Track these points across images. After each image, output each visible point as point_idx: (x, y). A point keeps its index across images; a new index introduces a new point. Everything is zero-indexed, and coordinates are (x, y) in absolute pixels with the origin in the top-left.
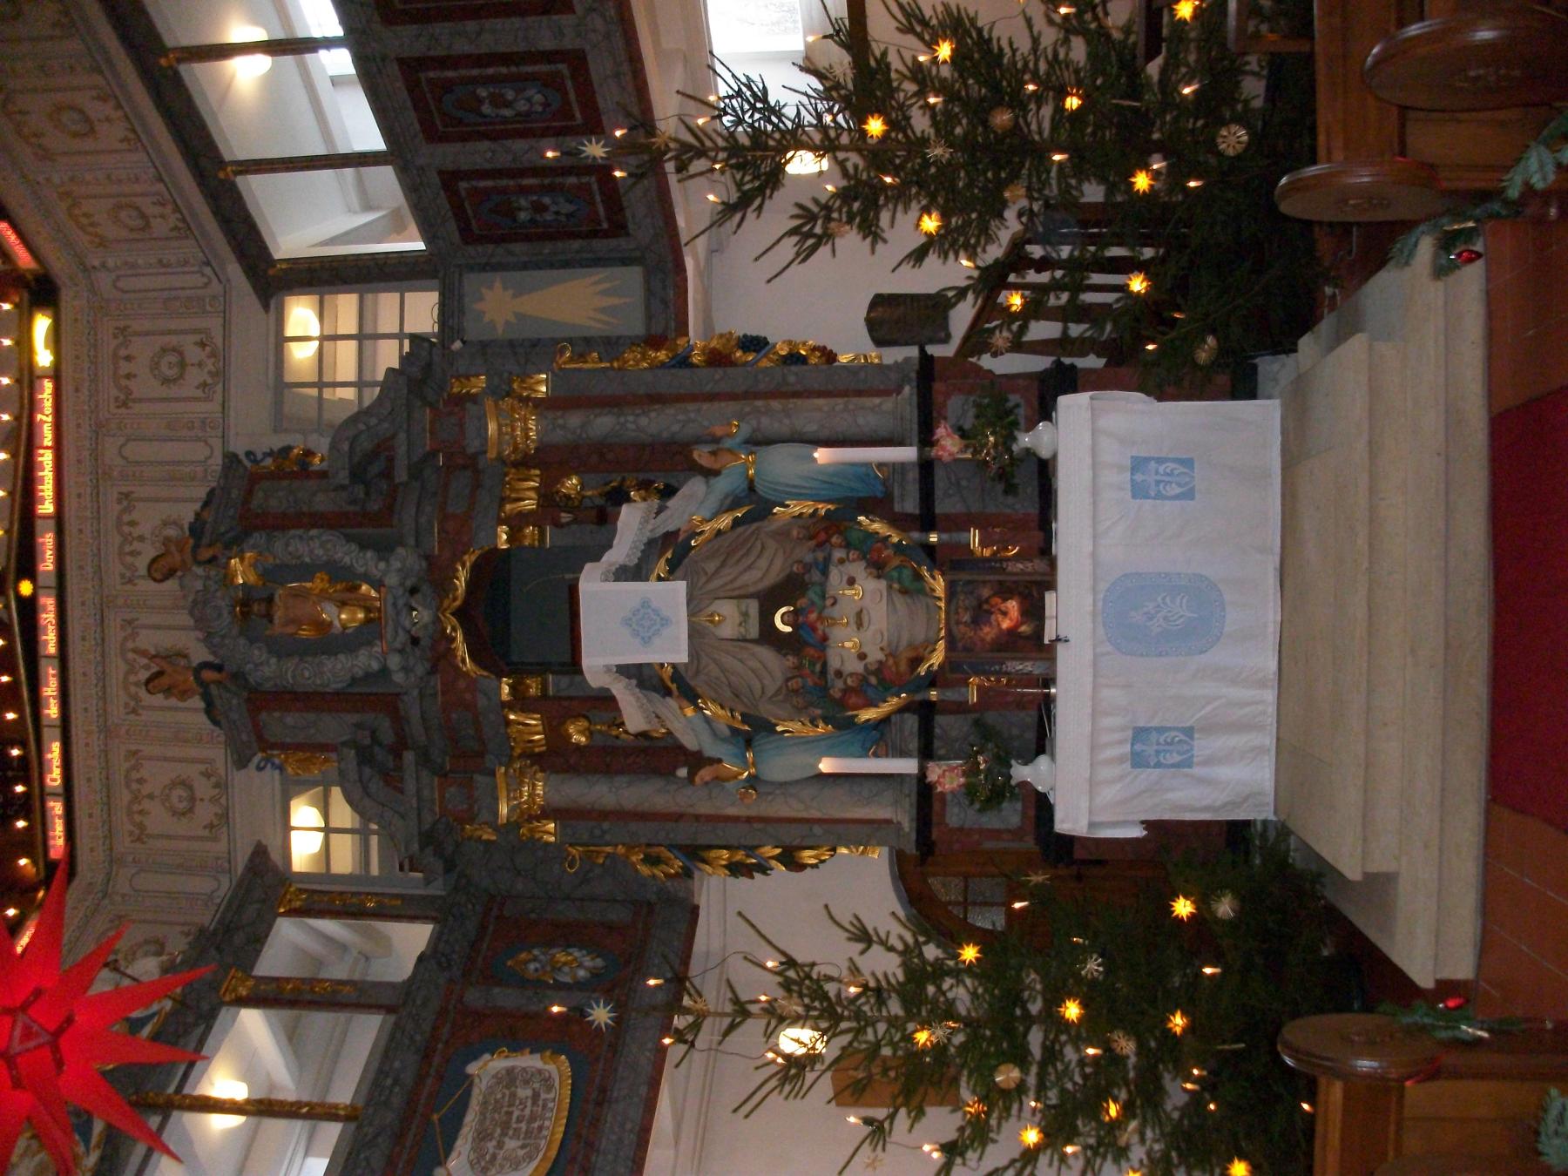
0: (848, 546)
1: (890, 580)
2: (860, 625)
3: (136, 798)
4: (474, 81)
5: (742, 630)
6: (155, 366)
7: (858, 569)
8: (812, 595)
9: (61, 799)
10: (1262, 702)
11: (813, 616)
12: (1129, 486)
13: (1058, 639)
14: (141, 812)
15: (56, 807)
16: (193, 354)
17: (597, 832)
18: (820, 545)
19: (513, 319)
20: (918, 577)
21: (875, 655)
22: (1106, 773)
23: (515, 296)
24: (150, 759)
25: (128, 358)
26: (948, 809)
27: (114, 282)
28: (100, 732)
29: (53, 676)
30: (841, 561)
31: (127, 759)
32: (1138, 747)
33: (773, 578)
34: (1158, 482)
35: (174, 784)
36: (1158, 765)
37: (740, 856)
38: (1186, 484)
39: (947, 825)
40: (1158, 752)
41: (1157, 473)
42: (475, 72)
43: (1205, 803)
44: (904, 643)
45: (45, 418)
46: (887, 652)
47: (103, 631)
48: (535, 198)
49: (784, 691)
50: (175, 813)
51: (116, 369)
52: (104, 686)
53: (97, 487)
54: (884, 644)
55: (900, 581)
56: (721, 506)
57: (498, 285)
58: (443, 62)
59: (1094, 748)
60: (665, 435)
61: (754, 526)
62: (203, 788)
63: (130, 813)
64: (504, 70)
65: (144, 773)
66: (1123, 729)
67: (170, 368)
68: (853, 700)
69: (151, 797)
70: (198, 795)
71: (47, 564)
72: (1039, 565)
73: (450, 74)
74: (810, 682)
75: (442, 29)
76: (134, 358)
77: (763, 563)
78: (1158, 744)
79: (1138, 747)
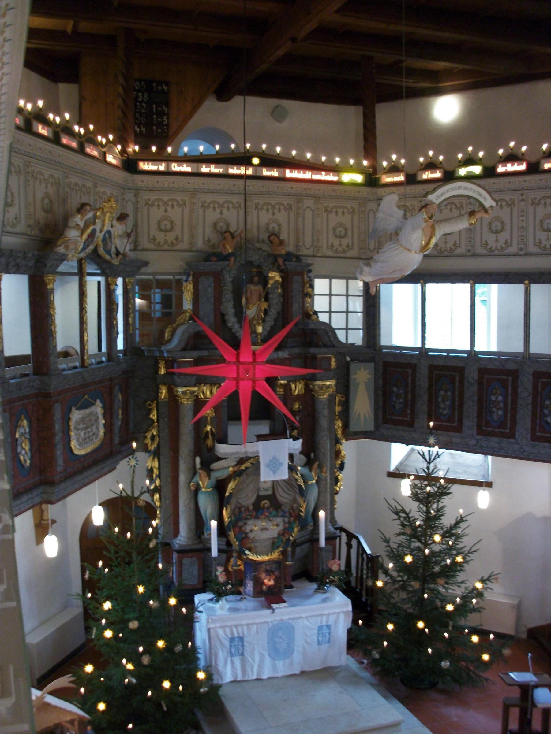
0: (289, 522)
1: (278, 538)
2: (262, 529)
3: (165, 204)
4: (453, 392)
5: (262, 489)
6: (341, 225)
7: (281, 527)
8: (274, 513)
9: (166, 170)
10: (253, 675)
11: (267, 514)
12: (321, 625)
13: (274, 610)
14: (159, 205)
15: (162, 167)
16: (345, 242)
17: (163, 416)
18: (290, 514)
19: (357, 381)
20: (278, 547)
21: (251, 535)
22: (228, 631)
23: (365, 383)
24: (183, 212)
25: (343, 213)
26: (189, 559)
27: (372, 210)
28: (194, 189)
29: (219, 171)
30: (284, 521)
31: (182, 200)
32: (237, 639)
33: (280, 499)
34: (323, 634)
35: (172, 223)
36: (231, 646)
37: (156, 471)
38: (322, 642)
39: (183, 559)
40: (235, 645)
41: (326, 633)
42: (457, 393)
43: (218, 663)
44: (257, 545)
45: (323, 176)
46: (254, 539)
47: (236, 194)
48: (403, 396)
49: (240, 506)
50: (159, 222)
51: (340, 207)
52: (213, 193)
53: (294, 196)
54: (256, 538)
55: (278, 542)
56: (187, 344)
57: (369, 376)
58: (462, 382)
59: (236, 626)
60: (320, 446)
61: (298, 491)
62: (170, 237)
63: (158, 200)
64: (457, 404)
65: (176, 208)
66: (243, 633)
67: (339, 231)
68: (237, 530)
69: (166, 211)
70: (168, 234)
71: (266, 172)
72: (94, 402)
73: (457, 384)
74: (244, 515)
75: (475, 388)
76: (343, 215)
77: (285, 495)
78: (238, 645)
79: (237, 639)
